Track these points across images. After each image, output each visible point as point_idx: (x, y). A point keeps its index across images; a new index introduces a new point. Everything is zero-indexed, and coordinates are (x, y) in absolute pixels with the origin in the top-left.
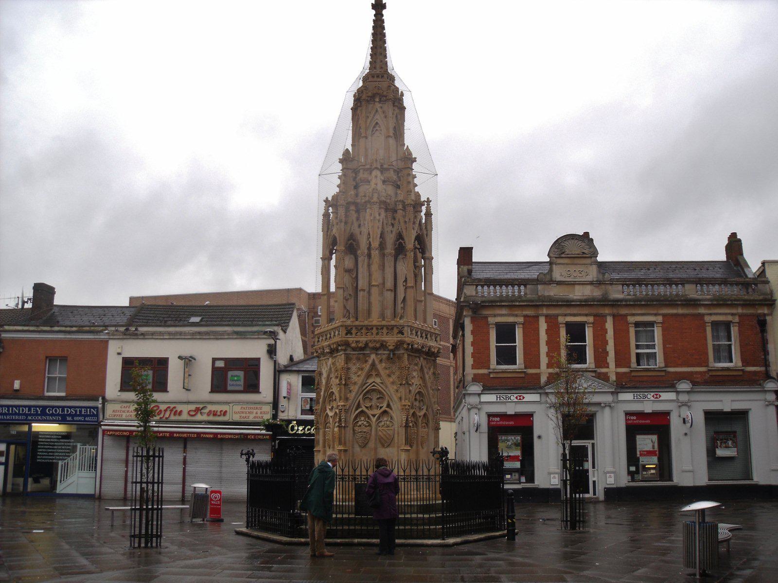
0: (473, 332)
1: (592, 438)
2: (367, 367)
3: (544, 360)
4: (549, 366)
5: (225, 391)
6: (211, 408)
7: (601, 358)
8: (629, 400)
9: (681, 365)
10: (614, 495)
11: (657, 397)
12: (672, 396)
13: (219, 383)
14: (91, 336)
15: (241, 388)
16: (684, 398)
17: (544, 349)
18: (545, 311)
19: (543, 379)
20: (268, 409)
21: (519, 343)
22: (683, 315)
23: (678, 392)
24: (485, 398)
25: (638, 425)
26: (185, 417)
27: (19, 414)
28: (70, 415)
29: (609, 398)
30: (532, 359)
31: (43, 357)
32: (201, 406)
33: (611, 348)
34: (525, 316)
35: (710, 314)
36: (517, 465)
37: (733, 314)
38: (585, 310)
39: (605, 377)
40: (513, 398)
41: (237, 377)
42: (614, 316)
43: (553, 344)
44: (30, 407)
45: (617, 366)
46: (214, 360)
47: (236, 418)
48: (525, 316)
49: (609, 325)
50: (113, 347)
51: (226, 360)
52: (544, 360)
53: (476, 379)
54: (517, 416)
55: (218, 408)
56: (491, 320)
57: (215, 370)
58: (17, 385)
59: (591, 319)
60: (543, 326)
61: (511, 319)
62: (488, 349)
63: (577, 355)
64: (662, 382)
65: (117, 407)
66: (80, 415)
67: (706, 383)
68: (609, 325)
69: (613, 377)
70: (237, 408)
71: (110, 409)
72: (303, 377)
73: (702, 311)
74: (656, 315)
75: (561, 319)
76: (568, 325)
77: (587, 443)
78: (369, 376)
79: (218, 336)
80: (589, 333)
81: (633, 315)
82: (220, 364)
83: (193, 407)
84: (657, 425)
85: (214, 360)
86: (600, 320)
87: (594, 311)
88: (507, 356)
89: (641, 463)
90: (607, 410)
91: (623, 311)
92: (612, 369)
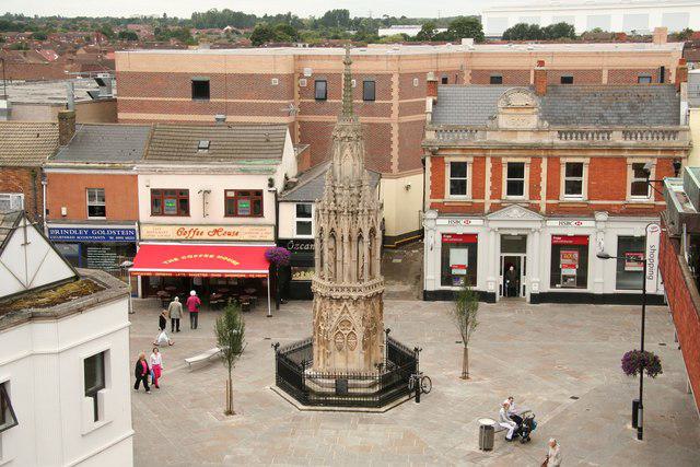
0: (432, 169)
1: (525, 252)
2: (342, 308)
3: (488, 193)
4: (492, 197)
5: (236, 215)
6: (226, 229)
7: (535, 194)
8: (557, 227)
9: (602, 199)
10: (538, 298)
11: (579, 224)
12: (592, 223)
13: (231, 208)
14: (123, 172)
15: (247, 213)
16: (601, 226)
17: (488, 184)
18: (491, 153)
19: (487, 208)
20: (272, 230)
21: (469, 178)
22: (607, 158)
23: (596, 222)
24: (439, 222)
25: (559, 246)
26: (205, 236)
27: (69, 235)
28: (112, 235)
29: (538, 225)
30: (479, 193)
31: (83, 188)
32: (217, 228)
33: (544, 184)
34: (475, 157)
35: (632, 157)
36: (464, 272)
37: (652, 157)
38: (525, 153)
39: (536, 209)
40: (462, 222)
41: (245, 204)
42: (549, 158)
43: (496, 180)
44: (78, 230)
45: (548, 198)
46: (226, 191)
47: (246, 237)
48: (475, 157)
49: (544, 165)
50: (142, 180)
51: (236, 191)
52: (488, 193)
53: (433, 207)
54: (465, 236)
55: (232, 229)
56: (447, 160)
57: (227, 199)
58: (64, 212)
59: (529, 160)
60: (489, 165)
61: (462, 160)
62: (443, 182)
63: (515, 188)
64: (586, 212)
65: (150, 228)
66: (121, 235)
67: (622, 214)
68: (544, 165)
69: (543, 208)
70: (247, 229)
71: (144, 229)
72: (298, 206)
73: (625, 154)
74: (584, 157)
75: (504, 160)
76: (510, 165)
77: (522, 255)
78: (342, 313)
79: (227, 172)
80: (527, 171)
81: (565, 156)
82: (232, 194)
83: (212, 229)
84: (580, 244)
85: (226, 191)
86: (536, 161)
87: (532, 153)
88: (459, 188)
89: (563, 273)
90: (536, 234)
91: (556, 154)
92: (543, 202)
